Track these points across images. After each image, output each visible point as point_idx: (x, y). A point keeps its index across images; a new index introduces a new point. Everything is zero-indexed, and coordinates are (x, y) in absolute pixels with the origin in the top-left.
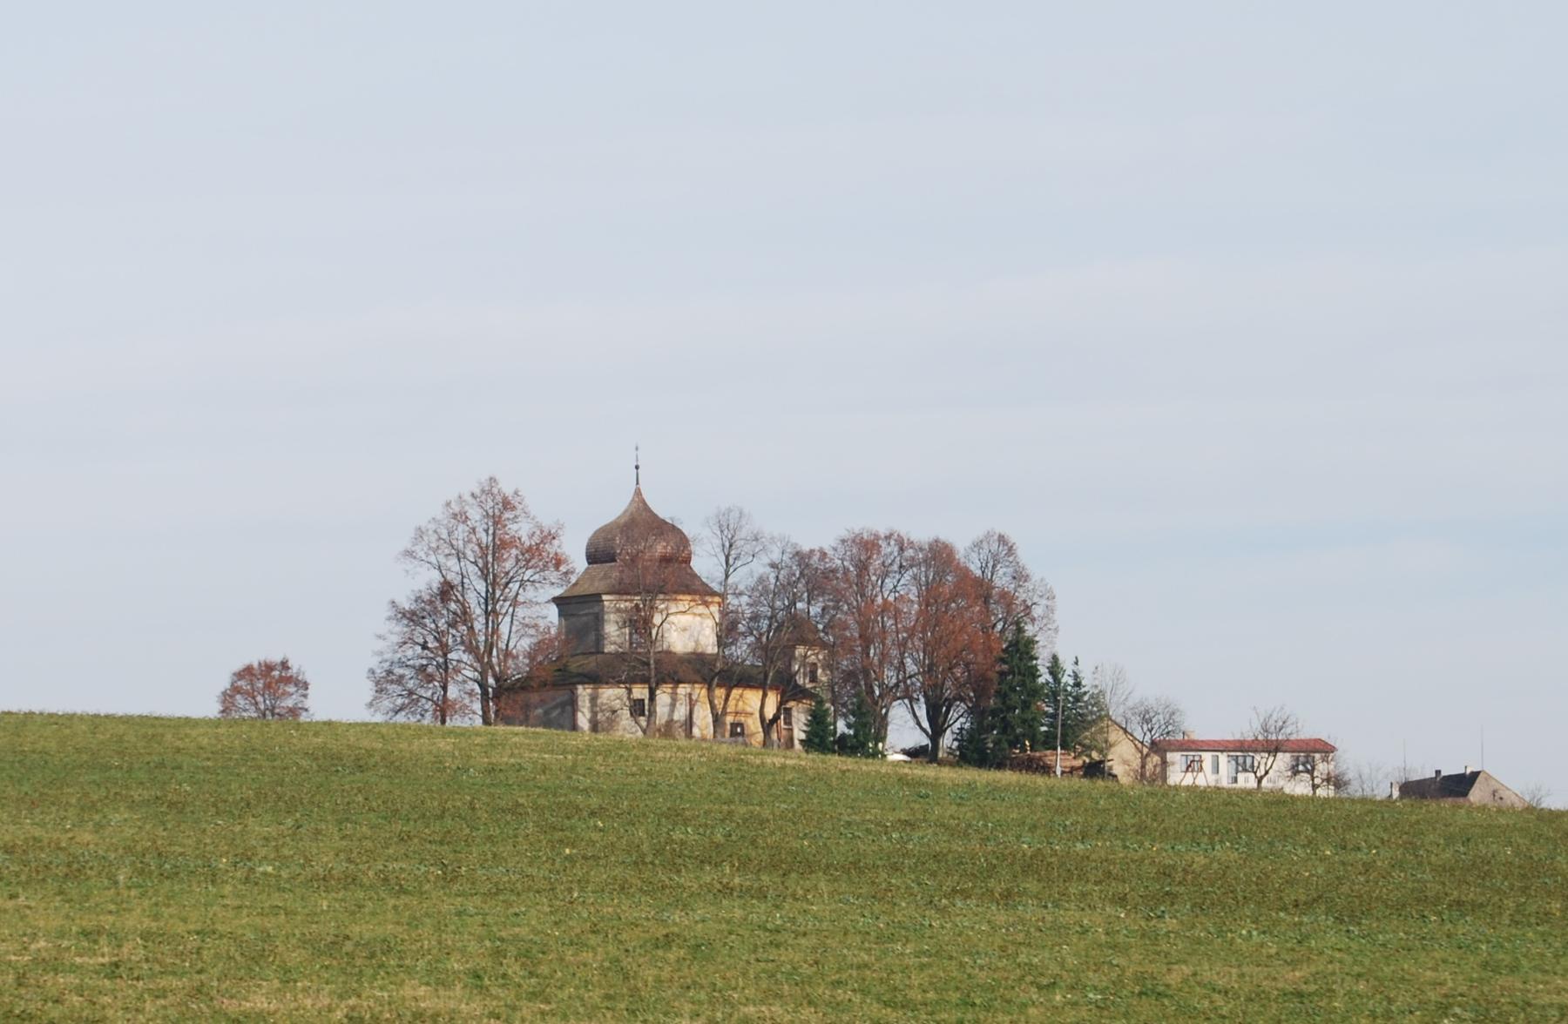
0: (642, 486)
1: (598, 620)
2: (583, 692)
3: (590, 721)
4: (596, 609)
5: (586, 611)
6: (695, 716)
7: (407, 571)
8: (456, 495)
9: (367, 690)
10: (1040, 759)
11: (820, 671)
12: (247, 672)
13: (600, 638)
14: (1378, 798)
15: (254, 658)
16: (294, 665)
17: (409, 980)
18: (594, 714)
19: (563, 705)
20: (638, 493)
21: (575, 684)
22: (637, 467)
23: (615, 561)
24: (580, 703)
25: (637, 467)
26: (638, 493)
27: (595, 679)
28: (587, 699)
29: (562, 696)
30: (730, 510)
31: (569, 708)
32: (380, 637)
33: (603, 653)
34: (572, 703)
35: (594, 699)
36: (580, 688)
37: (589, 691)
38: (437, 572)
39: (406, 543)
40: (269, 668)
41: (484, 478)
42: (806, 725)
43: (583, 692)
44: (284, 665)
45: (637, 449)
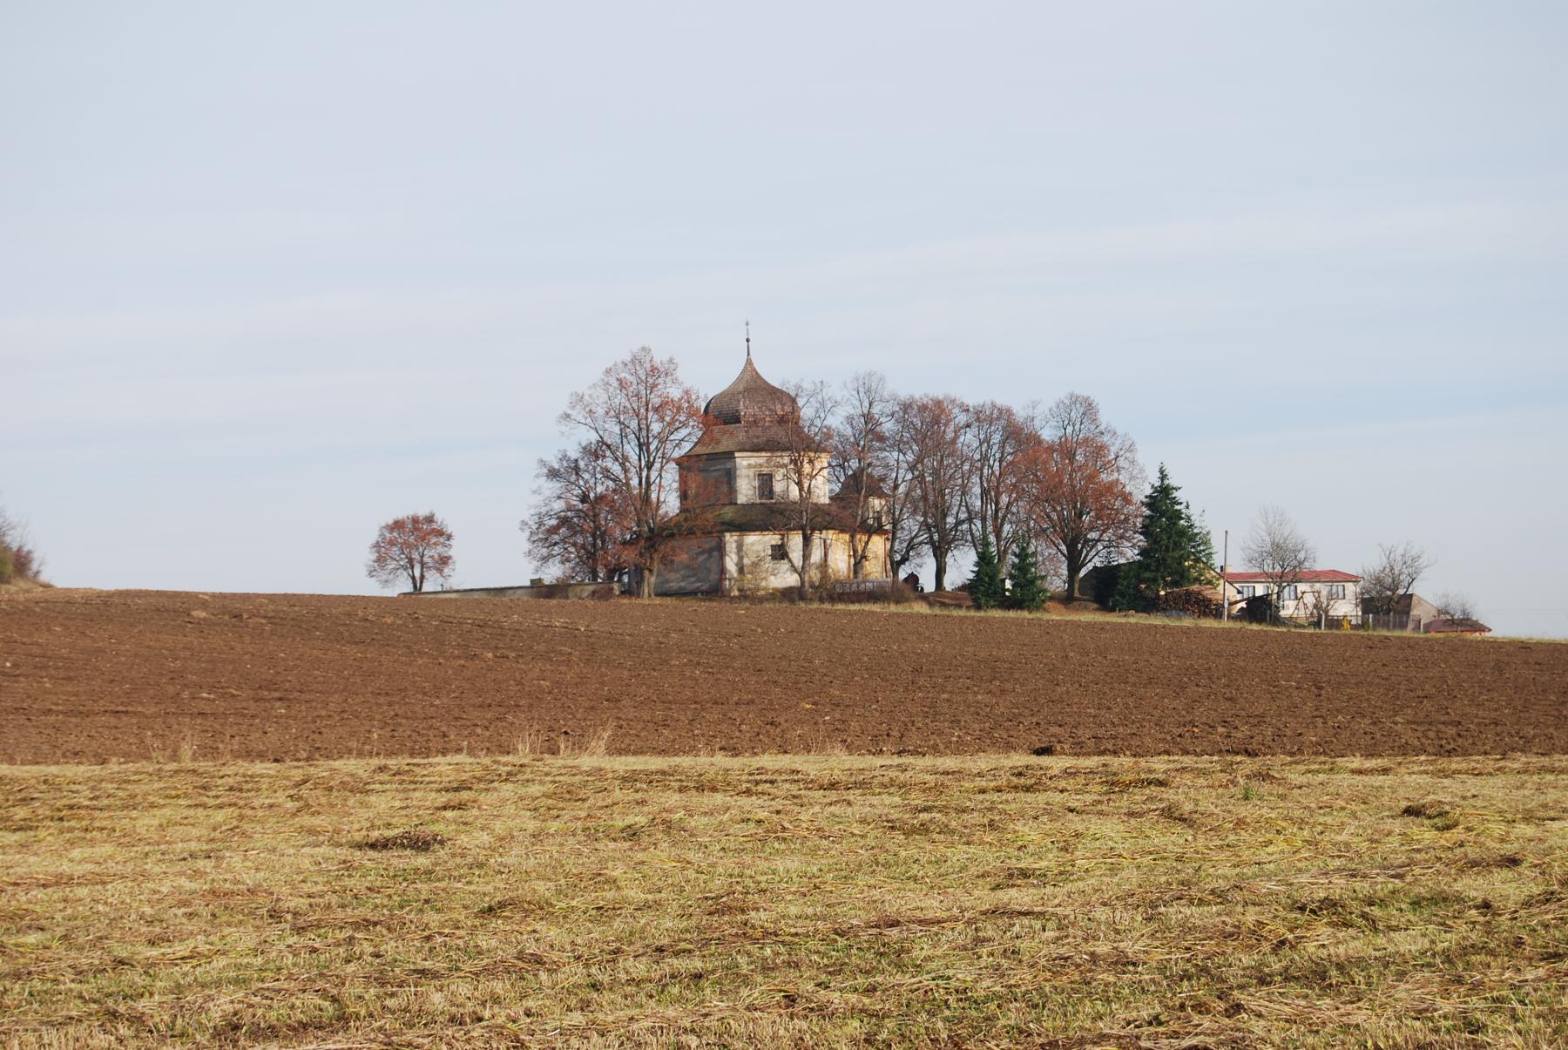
0: (752, 357)
1: (730, 476)
2: (731, 539)
3: (737, 565)
4: (728, 465)
5: (718, 467)
6: (829, 559)
7: (563, 433)
8: (668, 359)
9: (522, 542)
10: (1199, 593)
11: (884, 519)
12: (398, 525)
13: (732, 491)
14: (547, 582)
15: (403, 512)
16: (438, 517)
17: (1495, 960)
18: (741, 558)
19: (710, 551)
20: (749, 362)
21: (723, 532)
22: (748, 340)
23: (740, 422)
24: (727, 549)
25: (748, 340)
26: (749, 362)
27: (743, 527)
28: (734, 545)
29: (710, 543)
30: (870, 375)
31: (716, 554)
32: (535, 492)
33: (736, 504)
34: (721, 549)
35: (740, 547)
36: (728, 535)
37: (735, 538)
38: (593, 432)
39: (564, 407)
40: (415, 520)
41: (636, 348)
42: (975, 565)
43: (731, 539)
44: (430, 519)
45: (747, 324)
